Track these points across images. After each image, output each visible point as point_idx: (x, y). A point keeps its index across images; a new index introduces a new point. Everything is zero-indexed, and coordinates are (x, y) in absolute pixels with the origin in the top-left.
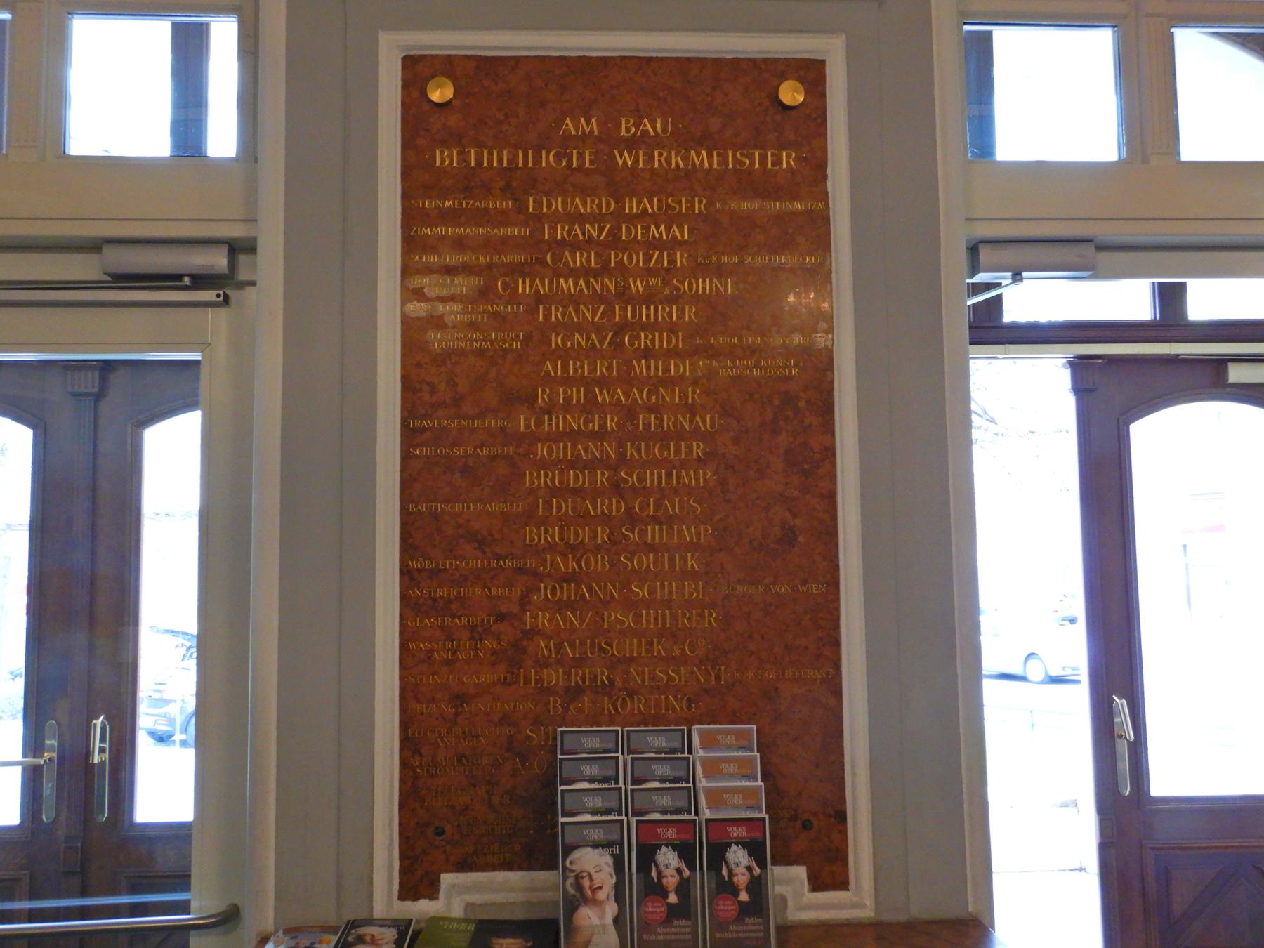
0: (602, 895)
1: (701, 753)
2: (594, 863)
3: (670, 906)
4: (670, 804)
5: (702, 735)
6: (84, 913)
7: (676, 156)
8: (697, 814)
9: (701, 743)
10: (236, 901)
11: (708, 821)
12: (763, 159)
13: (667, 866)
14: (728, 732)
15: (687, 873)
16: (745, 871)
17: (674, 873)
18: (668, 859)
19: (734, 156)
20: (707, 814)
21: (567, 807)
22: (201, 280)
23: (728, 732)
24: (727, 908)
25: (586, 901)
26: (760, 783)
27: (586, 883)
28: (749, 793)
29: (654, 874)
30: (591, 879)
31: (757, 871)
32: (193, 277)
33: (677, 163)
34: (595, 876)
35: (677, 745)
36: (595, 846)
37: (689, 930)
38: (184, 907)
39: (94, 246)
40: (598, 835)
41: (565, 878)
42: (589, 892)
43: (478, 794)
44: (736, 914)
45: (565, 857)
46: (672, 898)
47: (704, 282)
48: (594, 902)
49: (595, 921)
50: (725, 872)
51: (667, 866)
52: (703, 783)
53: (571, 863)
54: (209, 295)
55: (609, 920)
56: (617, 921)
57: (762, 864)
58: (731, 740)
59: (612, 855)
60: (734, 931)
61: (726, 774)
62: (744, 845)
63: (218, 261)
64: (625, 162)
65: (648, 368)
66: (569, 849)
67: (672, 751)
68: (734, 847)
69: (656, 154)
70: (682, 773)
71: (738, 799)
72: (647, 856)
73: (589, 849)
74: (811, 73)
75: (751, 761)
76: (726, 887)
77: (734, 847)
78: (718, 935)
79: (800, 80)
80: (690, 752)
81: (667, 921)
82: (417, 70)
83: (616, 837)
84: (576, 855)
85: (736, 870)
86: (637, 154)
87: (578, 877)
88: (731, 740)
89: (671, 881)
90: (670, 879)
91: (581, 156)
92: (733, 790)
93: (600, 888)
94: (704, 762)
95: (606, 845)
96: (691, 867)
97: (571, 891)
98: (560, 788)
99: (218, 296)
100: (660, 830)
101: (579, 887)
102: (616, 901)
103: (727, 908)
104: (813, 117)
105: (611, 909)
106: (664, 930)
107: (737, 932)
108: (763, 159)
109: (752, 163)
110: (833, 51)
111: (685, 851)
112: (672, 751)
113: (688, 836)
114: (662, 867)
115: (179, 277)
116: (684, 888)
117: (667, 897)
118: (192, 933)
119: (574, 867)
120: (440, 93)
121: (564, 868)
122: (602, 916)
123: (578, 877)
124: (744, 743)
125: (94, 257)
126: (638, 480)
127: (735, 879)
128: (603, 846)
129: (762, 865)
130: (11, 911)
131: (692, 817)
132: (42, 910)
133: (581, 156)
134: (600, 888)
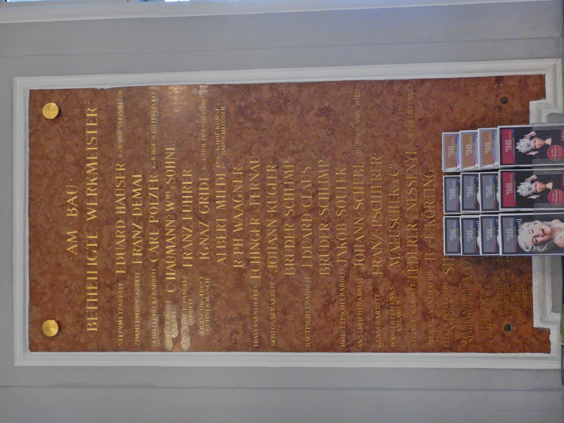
1: (459, 166)
5: (447, 166)
14: (447, 151)
23: (447, 151)
33: (94, 182)
36: (517, 233)
58: (451, 149)
59: (523, 223)
66: (519, 249)
67: (458, 184)
70: (472, 179)
73: (519, 237)
75: (464, 136)
83: (511, 221)
88: (451, 149)
95: (517, 226)
109: (94, 135)
112: (458, 184)
128: (517, 228)
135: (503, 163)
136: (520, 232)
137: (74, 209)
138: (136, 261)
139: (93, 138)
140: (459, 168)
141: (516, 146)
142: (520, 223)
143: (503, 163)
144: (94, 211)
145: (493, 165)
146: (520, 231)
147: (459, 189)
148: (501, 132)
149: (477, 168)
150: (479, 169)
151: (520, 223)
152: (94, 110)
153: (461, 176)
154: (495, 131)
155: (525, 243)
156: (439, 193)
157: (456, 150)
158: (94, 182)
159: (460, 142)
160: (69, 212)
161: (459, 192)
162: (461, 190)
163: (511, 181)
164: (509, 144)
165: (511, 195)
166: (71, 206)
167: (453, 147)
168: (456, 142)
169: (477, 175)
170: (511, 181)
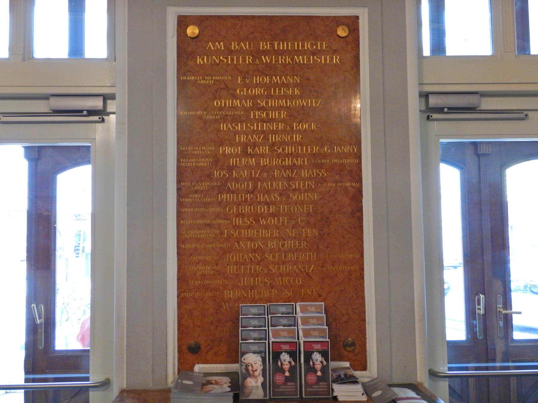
0: (256, 373)
1: (301, 314)
2: (253, 360)
3: (286, 377)
4: (257, 336)
5: (301, 307)
6: (487, 368)
7: (289, 58)
10: (108, 377)
11: (272, 342)
12: (325, 59)
13: (317, 360)
14: (311, 306)
15: (293, 363)
16: (320, 363)
17: (288, 363)
18: (285, 358)
19: (313, 58)
20: (272, 340)
22: (91, 112)
23: (311, 306)
24: (312, 378)
25: (250, 375)
27: (250, 368)
29: (279, 364)
30: (252, 367)
31: (325, 363)
32: (88, 111)
34: (254, 365)
36: (254, 353)
37: (294, 387)
38: (87, 379)
39: (46, 97)
40: (255, 348)
41: (241, 365)
42: (251, 372)
43: (207, 333)
44: (316, 381)
45: (241, 357)
46: (319, 374)
47: (275, 105)
48: (254, 376)
49: (254, 384)
50: (311, 363)
51: (317, 360)
52: (301, 327)
53: (244, 359)
54: (96, 118)
55: (259, 384)
56: (264, 385)
57: (327, 360)
59: (261, 357)
60: (315, 388)
61: (308, 322)
62: (320, 352)
63: (98, 103)
64: (266, 61)
66: (243, 354)
68: (315, 353)
70: (292, 323)
72: (276, 356)
73: (252, 354)
74: (352, 23)
76: (311, 370)
77: (315, 353)
78: (308, 389)
79: (347, 26)
80: (296, 314)
81: (317, 383)
82: (183, 22)
83: (263, 349)
84: (246, 356)
85: (284, 363)
86: (272, 57)
87: (247, 366)
88: (313, 309)
89: (318, 366)
90: (286, 366)
93: (256, 370)
94: (302, 318)
95: (259, 353)
96: (295, 361)
97: (244, 371)
98: (240, 329)
99: (100, 118)
100: (282, 346)
101: (247, 370)
102: (263, 376)
103: (312, 378)
105: (261, 379)
106: (283, 387)
107: (284, 388)
108: (325, 59)
110: (364, 16)
111: (293, 355)
112: (288, 313)
113: (294, 348)
114: (283, 361)
115: (81, 111)
116: (292, 369)
117: (317, 373)
118: (90, 389)
119: (245, 361)
120: (192, 31)
121: (241, 361)
122: (257, 382)
123: (247, 366)
125: (46, 102)
127: (316, 366)
128: (258, 353)
129: (327, 360)
130: (509, 366)
131: (296, 340)
132: (535, 366)
134: (256, 370)
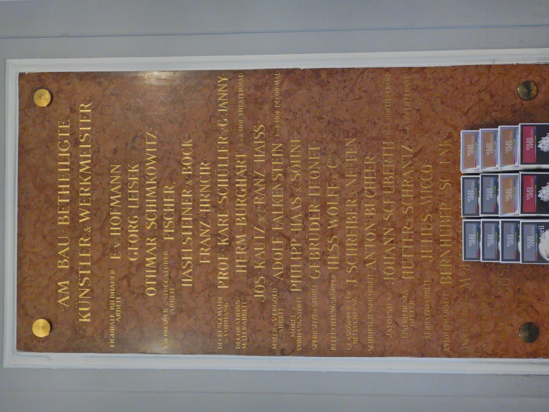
1: (479, 167)
5: (466, 166)
8: (478, 174)
9: (472, 167)
12: (85, 125)
14: (466, 150)
21: (475, 257)
23: (466, 150)
26: (519, 126)
28: (486, 140)
33: (87, 181)
35: (473, 183)
36: (538, 241)
58: (471, 147)
59: (545, 230)
65: (205, 203)
66: (539, 258)
67: (477, 186)
69: (60, 267)
70: (492, 180)
71: (489, 146)
73: (540, 245)
75: (484, 134)
82: (27, 343)
83: (533, 228)
86: (81, 207)
88: (471, 147)
91: (63, 131)
92: (484, 149)
94: (485, 165)
95: (538, 234)
104: (57, 82)
108: (85, 125)
109: (87, 131)
112: (477, 186)
120: (40, 328)
124: (492, 136)
126: (390, 209)
128: (539, 236)
133: (63, 131)
135: (524, 211)
136: (541, 240)
137: (65, 260)
138: (132, 198)
139: (87, 134)
140: (479, 168)
141: (538, 193)
142: (542, 230)
143: (524, 211)
144: (87, 212)
145: (514, 214)
146: (542, 239)
147: (479, 234)
148: (522, 179)
149: (498, 168)
150: (499, 170)
151: (542, 230)
152: (88, 189)
153: (480, 176)
154: (517, 128)
155: (546, 252)
156: (457, 239)
157: (476, 148)
158: (87, 181)
159: (480, 141)
160: (60, 264)
161: (479, 238)
162: (480, 192)
163: (532, 136)
164: (530, 191)
165: (532, 199)
166: (62, 258)
167: (472, 146)
168: (476, 140)
169: (497, 177)
170: (532, 136)
